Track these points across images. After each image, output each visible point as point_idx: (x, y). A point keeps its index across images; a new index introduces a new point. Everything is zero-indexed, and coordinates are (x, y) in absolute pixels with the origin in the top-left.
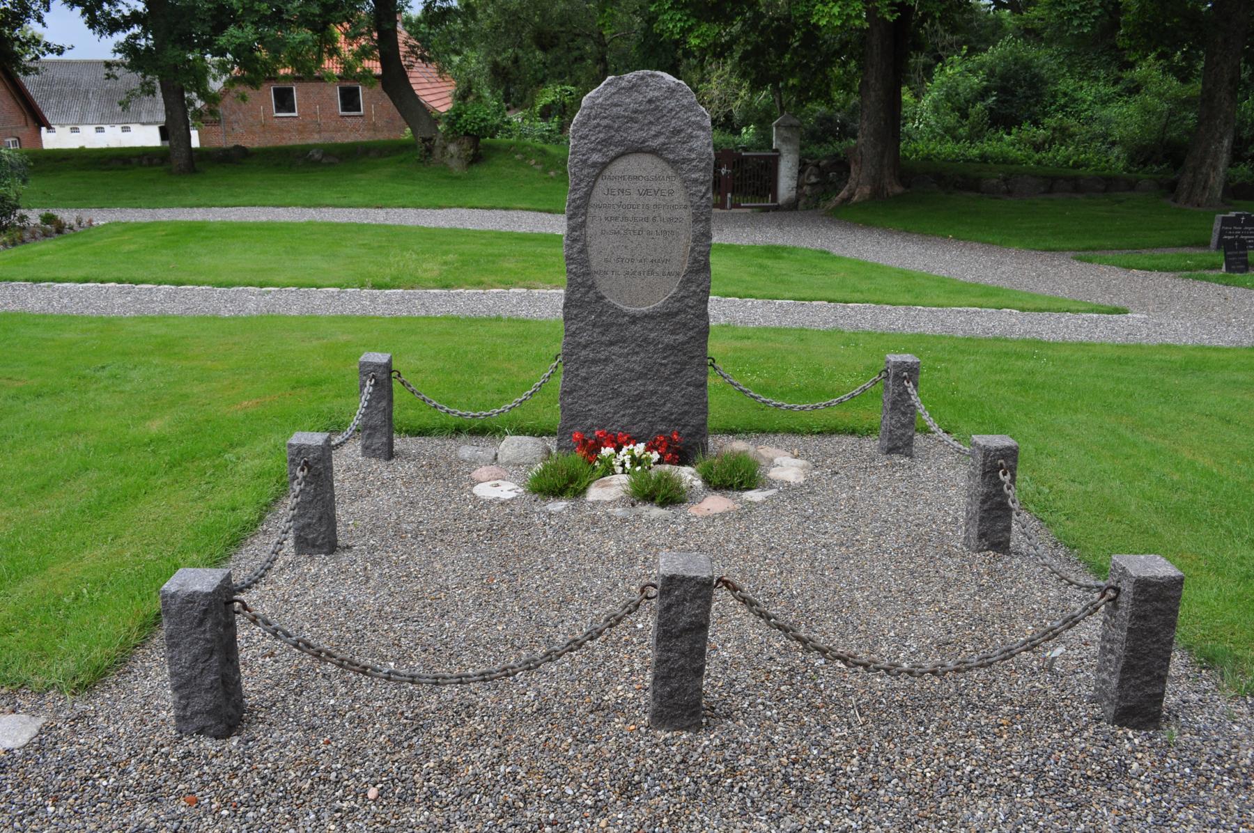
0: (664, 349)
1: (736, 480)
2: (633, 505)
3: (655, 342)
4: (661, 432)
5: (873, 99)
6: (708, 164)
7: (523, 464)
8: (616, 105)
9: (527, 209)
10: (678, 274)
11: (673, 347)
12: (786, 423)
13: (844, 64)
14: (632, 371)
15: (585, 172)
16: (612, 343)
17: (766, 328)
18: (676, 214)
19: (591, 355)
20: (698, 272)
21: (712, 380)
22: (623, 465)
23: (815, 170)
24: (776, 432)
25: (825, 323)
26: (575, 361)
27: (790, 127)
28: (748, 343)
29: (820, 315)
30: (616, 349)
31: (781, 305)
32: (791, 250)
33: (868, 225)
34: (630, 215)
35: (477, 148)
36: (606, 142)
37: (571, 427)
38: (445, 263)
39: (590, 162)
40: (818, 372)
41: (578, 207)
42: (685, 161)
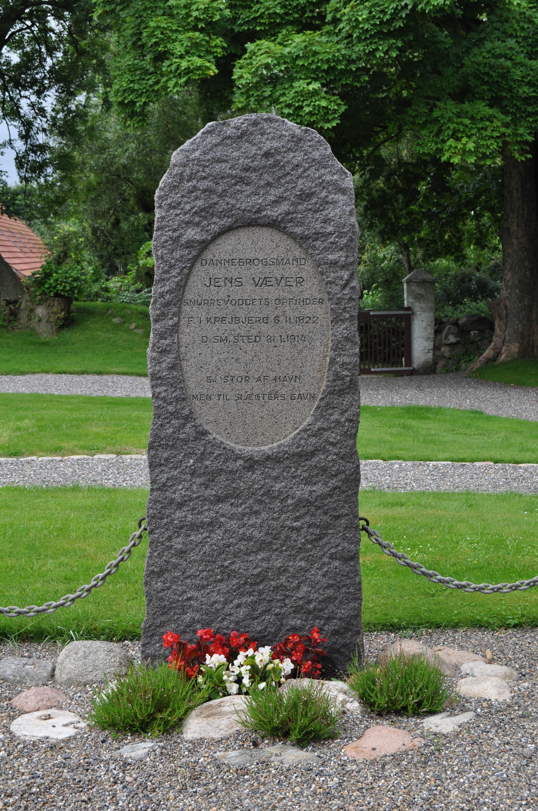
0: (296, 506)
1: (412, 700)
2: (255, 745)
3: (281, 496)
4: (295, 629)
5: (516, 247)
6: (351, 240)
7: (90, 683)
8: (219, 161)
9: (124, 374)
10: (313, 397)
11: (309, 503)
12: (468, 613)
13: (478, 217)
14: (250, 539)
15: (177, 254)
16: (219, 500)
17: (423, 493)
18: (308, 311)
19: (190, 517)
20: (341, 393)
21: (368, 555)
22: (239, 680)
23: (454, 329)
24: (455, 627)
25: (495, 487)
26: (167, 527)
27: (423, 282)
28: (401, 510)
29: (485, 477)
30: (225, 507)
31: (436, 467)
32: (439, 411)
33: (520, 384)
34: (242, 314)
35: (69, 312)
36: (205, 212)
37: (162, 625)
38: (19, 429)
39: (183, 240)
40: (499, 544)
41: (167, 304)
42: (318, 236)
